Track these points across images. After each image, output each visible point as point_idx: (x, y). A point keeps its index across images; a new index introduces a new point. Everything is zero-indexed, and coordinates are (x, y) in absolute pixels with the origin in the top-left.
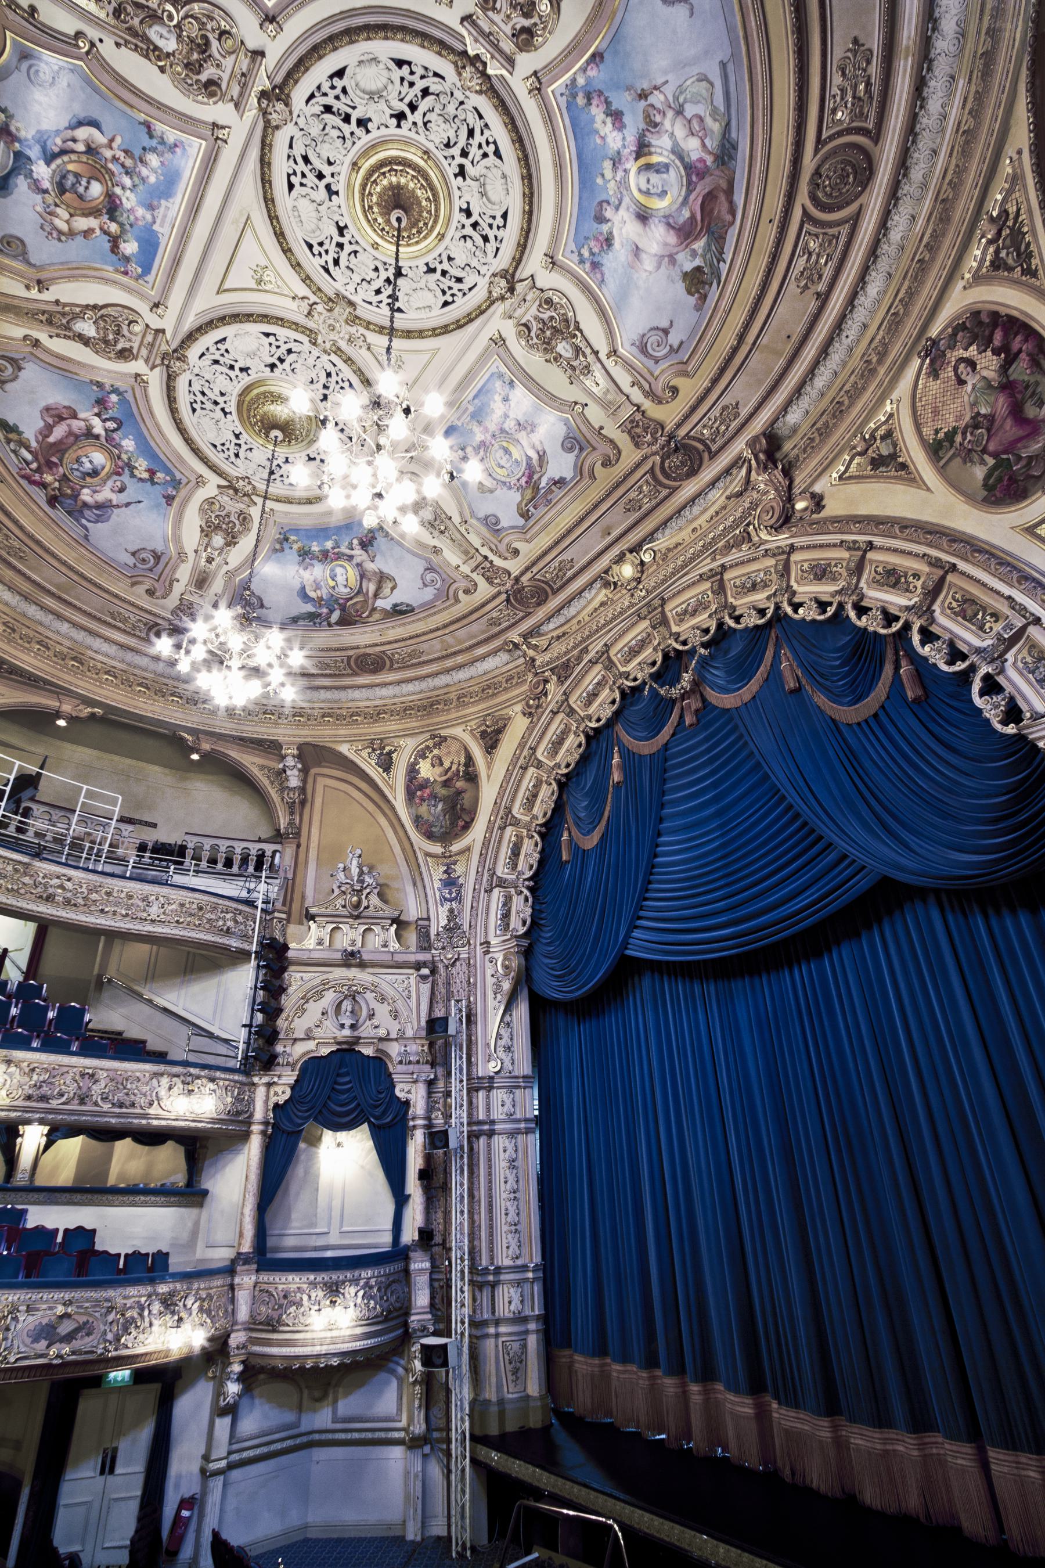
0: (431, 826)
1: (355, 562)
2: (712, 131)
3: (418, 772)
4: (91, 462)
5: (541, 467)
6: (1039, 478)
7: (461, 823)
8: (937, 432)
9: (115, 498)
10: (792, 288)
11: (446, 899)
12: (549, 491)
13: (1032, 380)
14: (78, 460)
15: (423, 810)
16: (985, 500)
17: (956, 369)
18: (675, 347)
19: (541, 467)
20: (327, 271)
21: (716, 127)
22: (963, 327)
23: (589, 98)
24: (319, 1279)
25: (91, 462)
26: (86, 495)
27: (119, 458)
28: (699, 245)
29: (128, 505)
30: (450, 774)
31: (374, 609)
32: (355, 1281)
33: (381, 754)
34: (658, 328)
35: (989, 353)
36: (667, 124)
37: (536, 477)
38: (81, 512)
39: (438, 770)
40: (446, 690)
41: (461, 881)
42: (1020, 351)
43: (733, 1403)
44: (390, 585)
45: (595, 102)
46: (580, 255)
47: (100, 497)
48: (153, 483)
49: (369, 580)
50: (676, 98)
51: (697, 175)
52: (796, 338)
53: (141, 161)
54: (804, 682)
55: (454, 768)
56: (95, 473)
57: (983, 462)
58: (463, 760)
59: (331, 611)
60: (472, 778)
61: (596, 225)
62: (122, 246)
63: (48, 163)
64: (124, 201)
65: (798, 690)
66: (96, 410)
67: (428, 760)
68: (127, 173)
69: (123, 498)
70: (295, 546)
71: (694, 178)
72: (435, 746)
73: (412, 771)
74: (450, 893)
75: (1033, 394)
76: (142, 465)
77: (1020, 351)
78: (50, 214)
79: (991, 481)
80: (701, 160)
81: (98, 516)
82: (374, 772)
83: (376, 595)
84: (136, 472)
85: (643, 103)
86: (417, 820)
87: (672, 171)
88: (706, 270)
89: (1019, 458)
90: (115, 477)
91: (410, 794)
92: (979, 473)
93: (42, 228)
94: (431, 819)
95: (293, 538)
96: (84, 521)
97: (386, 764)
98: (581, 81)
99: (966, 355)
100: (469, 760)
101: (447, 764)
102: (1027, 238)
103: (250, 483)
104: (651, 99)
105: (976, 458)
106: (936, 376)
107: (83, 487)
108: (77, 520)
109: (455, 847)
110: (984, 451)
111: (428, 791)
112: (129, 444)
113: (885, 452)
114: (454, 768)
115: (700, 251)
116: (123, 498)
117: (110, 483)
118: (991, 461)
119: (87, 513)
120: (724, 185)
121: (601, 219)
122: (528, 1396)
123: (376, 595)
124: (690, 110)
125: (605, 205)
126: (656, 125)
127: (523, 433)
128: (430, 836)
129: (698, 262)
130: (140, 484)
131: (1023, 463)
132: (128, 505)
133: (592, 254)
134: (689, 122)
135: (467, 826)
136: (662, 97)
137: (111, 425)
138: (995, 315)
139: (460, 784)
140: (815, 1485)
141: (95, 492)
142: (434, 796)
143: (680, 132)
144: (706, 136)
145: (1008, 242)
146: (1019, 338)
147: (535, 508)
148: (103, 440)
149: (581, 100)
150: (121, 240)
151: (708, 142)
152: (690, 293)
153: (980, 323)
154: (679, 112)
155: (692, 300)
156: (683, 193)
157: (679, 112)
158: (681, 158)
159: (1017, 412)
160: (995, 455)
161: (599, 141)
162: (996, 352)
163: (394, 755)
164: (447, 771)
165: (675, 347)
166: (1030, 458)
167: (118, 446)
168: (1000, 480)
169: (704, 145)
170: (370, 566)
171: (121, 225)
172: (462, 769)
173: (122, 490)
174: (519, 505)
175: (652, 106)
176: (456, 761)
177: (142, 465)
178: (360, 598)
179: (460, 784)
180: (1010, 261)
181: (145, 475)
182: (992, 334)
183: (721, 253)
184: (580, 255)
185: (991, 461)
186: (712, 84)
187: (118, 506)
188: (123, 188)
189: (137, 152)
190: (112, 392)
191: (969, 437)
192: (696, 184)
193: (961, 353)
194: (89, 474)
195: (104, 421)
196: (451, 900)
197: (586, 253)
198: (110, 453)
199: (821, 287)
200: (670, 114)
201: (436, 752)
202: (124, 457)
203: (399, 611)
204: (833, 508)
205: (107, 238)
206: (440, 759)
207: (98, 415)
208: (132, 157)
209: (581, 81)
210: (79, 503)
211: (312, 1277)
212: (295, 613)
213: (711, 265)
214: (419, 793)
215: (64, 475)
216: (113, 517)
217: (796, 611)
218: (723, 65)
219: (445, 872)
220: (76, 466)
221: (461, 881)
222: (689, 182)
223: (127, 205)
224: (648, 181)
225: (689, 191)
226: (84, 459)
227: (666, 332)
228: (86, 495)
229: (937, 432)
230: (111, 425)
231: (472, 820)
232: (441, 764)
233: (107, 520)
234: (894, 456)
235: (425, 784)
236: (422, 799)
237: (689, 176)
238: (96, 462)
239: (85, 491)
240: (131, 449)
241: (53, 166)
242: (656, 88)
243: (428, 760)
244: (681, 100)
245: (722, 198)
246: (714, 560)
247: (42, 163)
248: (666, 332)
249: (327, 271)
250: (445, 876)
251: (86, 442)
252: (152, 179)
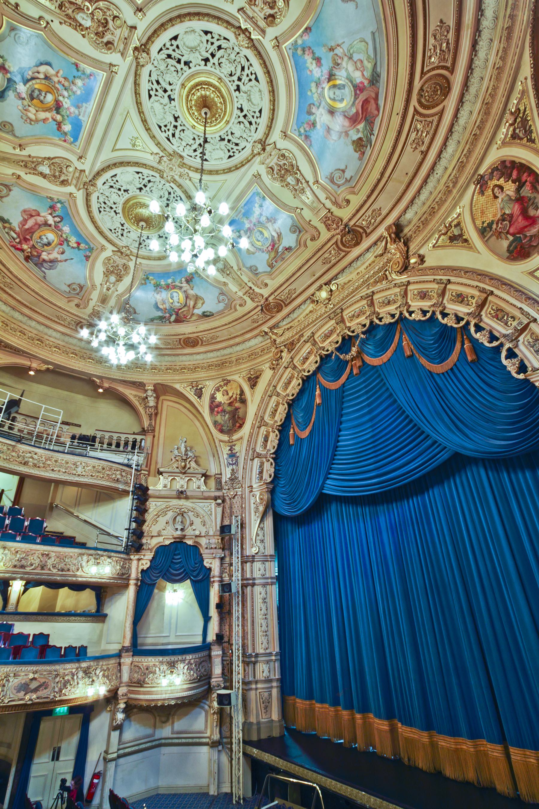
0: (222, 426)
1: (183, 290)
2: (367, 68)
3: (216, 398)
4: (47, 238)
5: (279, 241)
6: (536, 246)
7: (238, 425)
8: (483, 223)
9: (60, 257)
10: (409, 149)
11: (230, 464)
12: (283, 253)
13: (532, 196)
14: (40, 238)
15: (219, 418)
16: (508, 258)
17: (493, 190)
18: (348, 179)
19: (279, 241)
20: (169, 140)
21: (369, 66)
22: (496, 169)
23: (304, 51)
24: (165, 660)
25: (47, 238)
26: (44, 256)
27: (61, 236)
28: (361, 126)
29: (66, 260)
30: (232, 399)
31: (193, 314)
32: (183, 661)
33: (197, 389)
34: (339, 169)
35: (510, 182)
36: (344, 64)
37: (276, 246)
38: (42, 264)
39: (226, 397)
40: (230, 356)
41: (238, 454)
42: (526, 181)
43: (378, 724)
44: (201, 302)
45: (307, 53)
46: (299, 132)
47: (52, 257)
48: (79, 249)
49: (191, 299)
50: (349, 51)
51: (360, 90)
52: (410, 174)
53: (73, 83)
54: (414, 352)
55: (234, 396)
56: (49, 244)
57: (507, 238)
58: (239, 392)
59: (171, 315)
60: (243, 401)
61: (307, 116)
62: (63, 127)
63: (25, 84)
64: (64, 103)
65: (412, 356)
66: (50, 212)
67: (221, 392)
68: (66, 89)
69: (63, 257)
70: (152, 282)
71: (358, 92)
72: (224, 385)
73: (213, 398)
74: (232, 461)
75: (533, 203)
76: (73, 240)
77: (526, 181)
78: (25, 110)
79: (511, 248)
80: (362, 83)
81: (51, 266)
82: (193, 398)
83: (194, 307)
84: (70, 244)
85: (332, 53)
86: (215, 423)
87: (347, 89)
88: (364, 139)
89: (526, 236)
90: (60, 246)
91: (212, 409)
92: (505, 244)
93: (22, 117)
94: (222, 423)
95: (151, 277)
96: (43, 269)
97: (199, 394)
98: (300, 42)
99: (498, 183)
100: (242, 392)
101: (230, 394)
102: (530, 123)
103: (129, 249)
104: (336, 51)
105: (503, 236)
106: (483, 194)
107: (43, 251)
108: (40, 268)
109: (235, 437)
110: (508, 233)
111: (220, 408)
112: (66, 229)
113: (456, 233)
114: (234, 396)
115: (361, 130)
116: (63, 257)
117: (57, 249)
118: (511, 238)
119: (45, 265)
120: (373, 95)
121: (310, 113)
122: (272, 720)
123: (194, 307)
124: (356, 57)
125: (312, 106)
126: (338, 64)
127: (270, 223)
128: (221, 431)
129: (360, 135)
130: (72, 250)
131: (528, 239)
132: (66, 260)
133: (306, 131)
134: (356, 63)
135: (241, 426)
136: (341, 50)
137: (58, 219)
138: (513, 163)
139: (237, 405)
140: (420, 766)
141: (49, 254)
142: (223, 411)
143: (351, 68)
144: (364, 70)
145: (520, 125)
146: (525, 175)
147: (276, 262)
148: (53, 227)
149: (299, 52)
150: (62, 124)
151: (365, 73)
152: (356, 151)
153: (506, 167)
154: (350, 58)
155: (357, 155)
156: (352, 100)
157: (350, 58)
158: (351, 82)
159: (524, 212)
160: (513, 235)
161: (309, 73)
162: (514, 182)
163: (203, 390)
164: (230, 398)
165: (348, 179)
166: (531, 236)
167: (61, 230)
168: (516, 247)
169: (363, 75)
170: (191, 292)
171: (63, 116)
172: (238, 397)
173: (63, 253)
174: (268, 260)
175: (336, 55)
176: (235, 393)
177: (73, 240)
178: (186, 309)
179: (237, 405)
180: (521, 135)
181: (75, 245)
182: (511, 172)
183: (372, 131)
184: (299, 132)
185: (511, 238)
186: (367, 43)
187: (61, 261)
188: (64, 97)
189: (71, 78)
190: (58, 202)
191: (500, 225)
192: (359, 95)
193: (496, 182)
194: (46, 245)
195: (54, 217)
196: (233, 464)
197: (302, 130)
198: (57, 234)
199: (424, 148)
200: (346, 59)
201: (225, 388)
202: (64, 236)
203: (206, 315)
204: (429, 262)
205: (55, 123)
206: (227, 392)
207: (51, 214)
208: (68, 81)
209: (300, 42)
210: (41, 260)
211: (161, 659)
212: (152, 316)
213: (367, 137)
214: (216, 409)
215: (33, 245)
216: (59, 267)
217: (410, 315)
218: (373, 34)
219: (230, 450)
220: (39, 241)
221: (238, 454)
222: (356, 94)
223: (65, 105)
224: (334, 93)
225: (356, 99)
226: (43, 237)
227: (343, 171)
228: (44, 256)
229: (483, 223)
230: (58, 219)
231: (244, 423)
232: (228, 394)
233: (55, 268)
234: (461, 235)
235: (219, 405)
236: (218, 412)
237: (355, 91)
238: (49, 238)
239: (44, 253)
240: (67, 232)
241: (28, 86)
242: (338, 45)
243: (221, 392)
244: (351, 52)
245: (372, 102)
246: (368, 289)
247: (22, 84)
248: (343, 171)
249: (169, 140)
250: (230, 452)
251: (45, 228)
252: (79, 92)
